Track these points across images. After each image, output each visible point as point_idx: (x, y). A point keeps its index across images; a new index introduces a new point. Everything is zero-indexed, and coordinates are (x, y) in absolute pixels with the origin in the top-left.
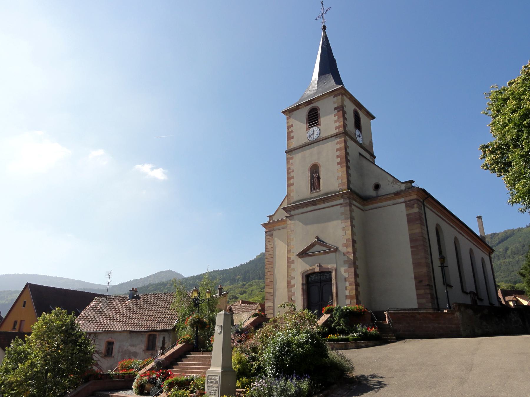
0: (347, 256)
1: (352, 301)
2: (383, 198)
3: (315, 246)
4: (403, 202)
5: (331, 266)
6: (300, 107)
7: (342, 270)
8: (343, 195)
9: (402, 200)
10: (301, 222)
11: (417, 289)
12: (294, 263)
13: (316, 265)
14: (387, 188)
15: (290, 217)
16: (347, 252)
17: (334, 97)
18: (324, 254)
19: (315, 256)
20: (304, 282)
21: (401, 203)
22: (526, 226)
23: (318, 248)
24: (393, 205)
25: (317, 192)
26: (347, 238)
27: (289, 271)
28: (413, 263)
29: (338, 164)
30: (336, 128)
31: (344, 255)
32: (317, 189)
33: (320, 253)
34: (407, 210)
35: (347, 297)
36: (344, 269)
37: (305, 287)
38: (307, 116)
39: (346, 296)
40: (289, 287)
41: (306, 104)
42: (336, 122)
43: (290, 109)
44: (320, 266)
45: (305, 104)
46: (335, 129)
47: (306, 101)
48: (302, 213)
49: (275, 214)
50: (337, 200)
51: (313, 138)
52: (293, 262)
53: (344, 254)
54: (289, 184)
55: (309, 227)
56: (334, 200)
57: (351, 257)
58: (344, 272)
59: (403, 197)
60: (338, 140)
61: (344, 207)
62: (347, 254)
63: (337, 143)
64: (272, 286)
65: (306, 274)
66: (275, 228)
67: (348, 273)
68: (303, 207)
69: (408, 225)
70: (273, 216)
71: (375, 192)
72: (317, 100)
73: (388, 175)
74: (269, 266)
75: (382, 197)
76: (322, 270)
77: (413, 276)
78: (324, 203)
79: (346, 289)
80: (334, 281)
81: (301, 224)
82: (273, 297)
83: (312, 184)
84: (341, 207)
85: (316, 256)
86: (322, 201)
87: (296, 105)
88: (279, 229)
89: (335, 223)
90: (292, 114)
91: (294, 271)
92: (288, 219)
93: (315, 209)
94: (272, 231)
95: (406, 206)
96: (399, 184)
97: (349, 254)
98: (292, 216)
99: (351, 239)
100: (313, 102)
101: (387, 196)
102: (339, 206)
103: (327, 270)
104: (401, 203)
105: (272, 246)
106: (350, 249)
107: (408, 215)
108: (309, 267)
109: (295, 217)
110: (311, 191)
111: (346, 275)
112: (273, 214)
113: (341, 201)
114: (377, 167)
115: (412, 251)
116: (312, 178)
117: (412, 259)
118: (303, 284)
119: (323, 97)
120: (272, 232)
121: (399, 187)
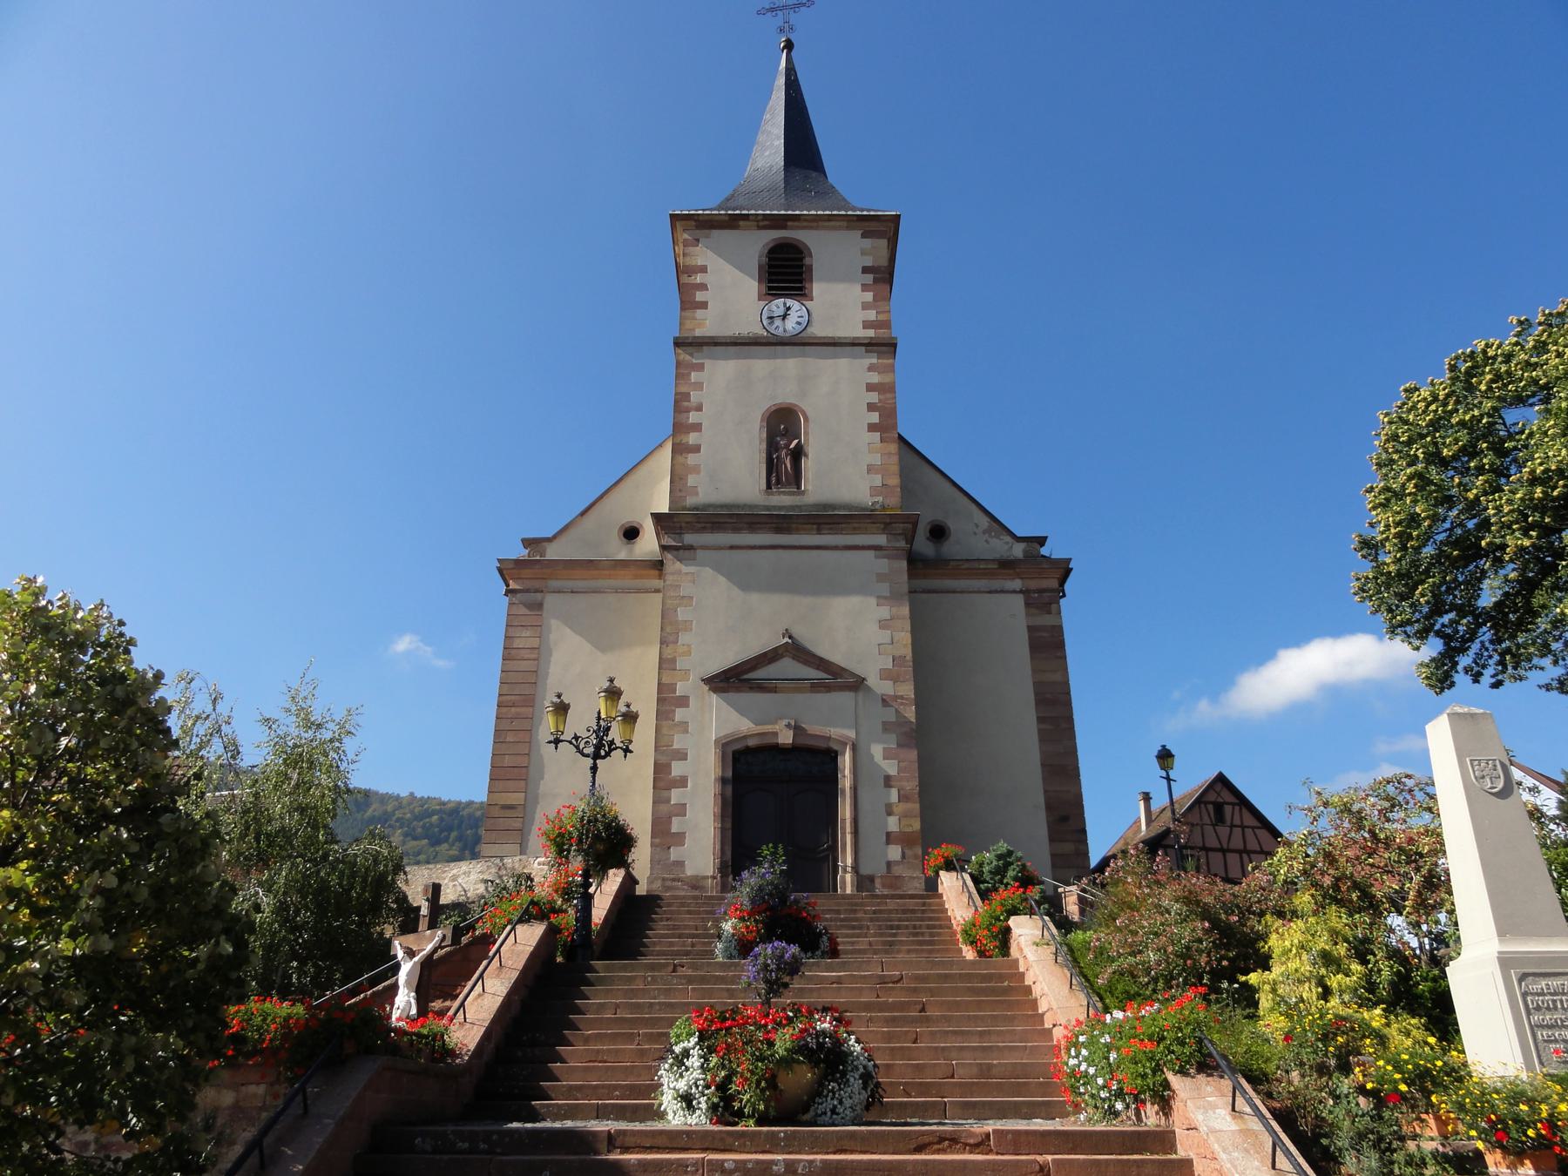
0: (896, 710)
1: (908, 852)
2: (966, 565)
3: (778, 660)
4: (1021, 592)
5: (839, 732)
6: (741, 223)
7: (877, 751)
8: (891, 523)
9: (1017, 584)
10: (722, 575)
11: (1053, 839)
12: (688, 706)
13: (785, 722)
14: (968, 540)
15: (681, 551)
16: (896, 697)
17: (864, 236)
18: (812, 692)
19: (776, 692)
20: (729, 774)
21: (1014, 592)
22: (1509, 686)
23: (788, 667)
24: (990, 592)
25: (793, 494)
26: (898, 653)
27: (665, 731)
28: (1042, 765)
29: (872, 428)
30: (867, 325)
31: (885, 702)
32: (788, 484)
33: (797, 685)
34: (1027, 615)
35: (890, 838)
36: (884, 748)
37: (729, 789)
38: (765, 260)
39: (888, 834)
40: (661, 784)
41: (766, 223)
42: (865, 306)
43: (706, 218)
44: (797, 729)
45: (763, 220)
46: (864, 327)
47: (768, 212)
48: (732, 547)
49: (555, 537)
50: (866, 532)
51: (781, 329)
52: (683, 702)
53: (884, 701)
54: (680, 444)
55: (755, 598)
56: (855, 529)
57: (910, 713)
58: (884, 759)
59: (1022, 578)
60: (874, 361)
61: (888, 557)
62: (894, 704)
63: (871, 368)
64: (523, 783)
65: (738, 746)
66: (554, 584)
67: (896, 762)
68: (736, 530)
69: (1032, 658)
70: (545, 544)
71: (930, 544)
72: (805, 224)
73: (973, 507)
74: (513, 709)
75: (961, 563)
76: (802, 741)
77: (1041, 800)
78: (819, 532)
79: (890, 813)
80: (846, 781)
81: (722, 579)
82: (523, 823)
83: (772, 466)
84: (876, 557)
85: (782, 692)
86: (813, 524)
87: (730, 212)
88: (572, 592)
89: (855, 601)
90: (707, 237)
91: (687, 732)
92: (669, 556)
93: (802, 544)
94: (542, 592)
95: (1027, 605)
96: (1008, 539)
97: (902, 704)
98: (691, 548)
99: (909, 657)
100: (789, 223)
101: (976, 565)
102: (871, 553)
103: (822, 745)
104: (1014, 592)
105: (535, 643)
106: (907, 690)
107: (1031, 629)
108: (752, 725)
109: (700, 553)
110: (769, 486)
111: (891, 768)
112: (550, 536)
113: (881, 540)
114: (938, 476)
115: (1040, 731)
116: (772, 447)
117: (1042, 752)
118: (723, 781)
119: (826, 224)
120: (539, 596)
121: (1006, 547)
